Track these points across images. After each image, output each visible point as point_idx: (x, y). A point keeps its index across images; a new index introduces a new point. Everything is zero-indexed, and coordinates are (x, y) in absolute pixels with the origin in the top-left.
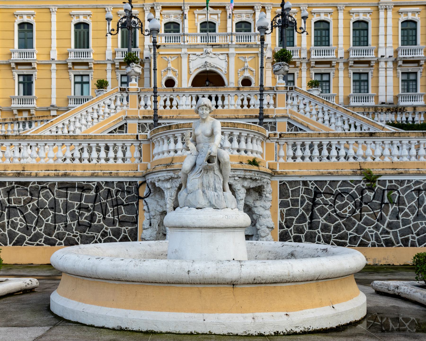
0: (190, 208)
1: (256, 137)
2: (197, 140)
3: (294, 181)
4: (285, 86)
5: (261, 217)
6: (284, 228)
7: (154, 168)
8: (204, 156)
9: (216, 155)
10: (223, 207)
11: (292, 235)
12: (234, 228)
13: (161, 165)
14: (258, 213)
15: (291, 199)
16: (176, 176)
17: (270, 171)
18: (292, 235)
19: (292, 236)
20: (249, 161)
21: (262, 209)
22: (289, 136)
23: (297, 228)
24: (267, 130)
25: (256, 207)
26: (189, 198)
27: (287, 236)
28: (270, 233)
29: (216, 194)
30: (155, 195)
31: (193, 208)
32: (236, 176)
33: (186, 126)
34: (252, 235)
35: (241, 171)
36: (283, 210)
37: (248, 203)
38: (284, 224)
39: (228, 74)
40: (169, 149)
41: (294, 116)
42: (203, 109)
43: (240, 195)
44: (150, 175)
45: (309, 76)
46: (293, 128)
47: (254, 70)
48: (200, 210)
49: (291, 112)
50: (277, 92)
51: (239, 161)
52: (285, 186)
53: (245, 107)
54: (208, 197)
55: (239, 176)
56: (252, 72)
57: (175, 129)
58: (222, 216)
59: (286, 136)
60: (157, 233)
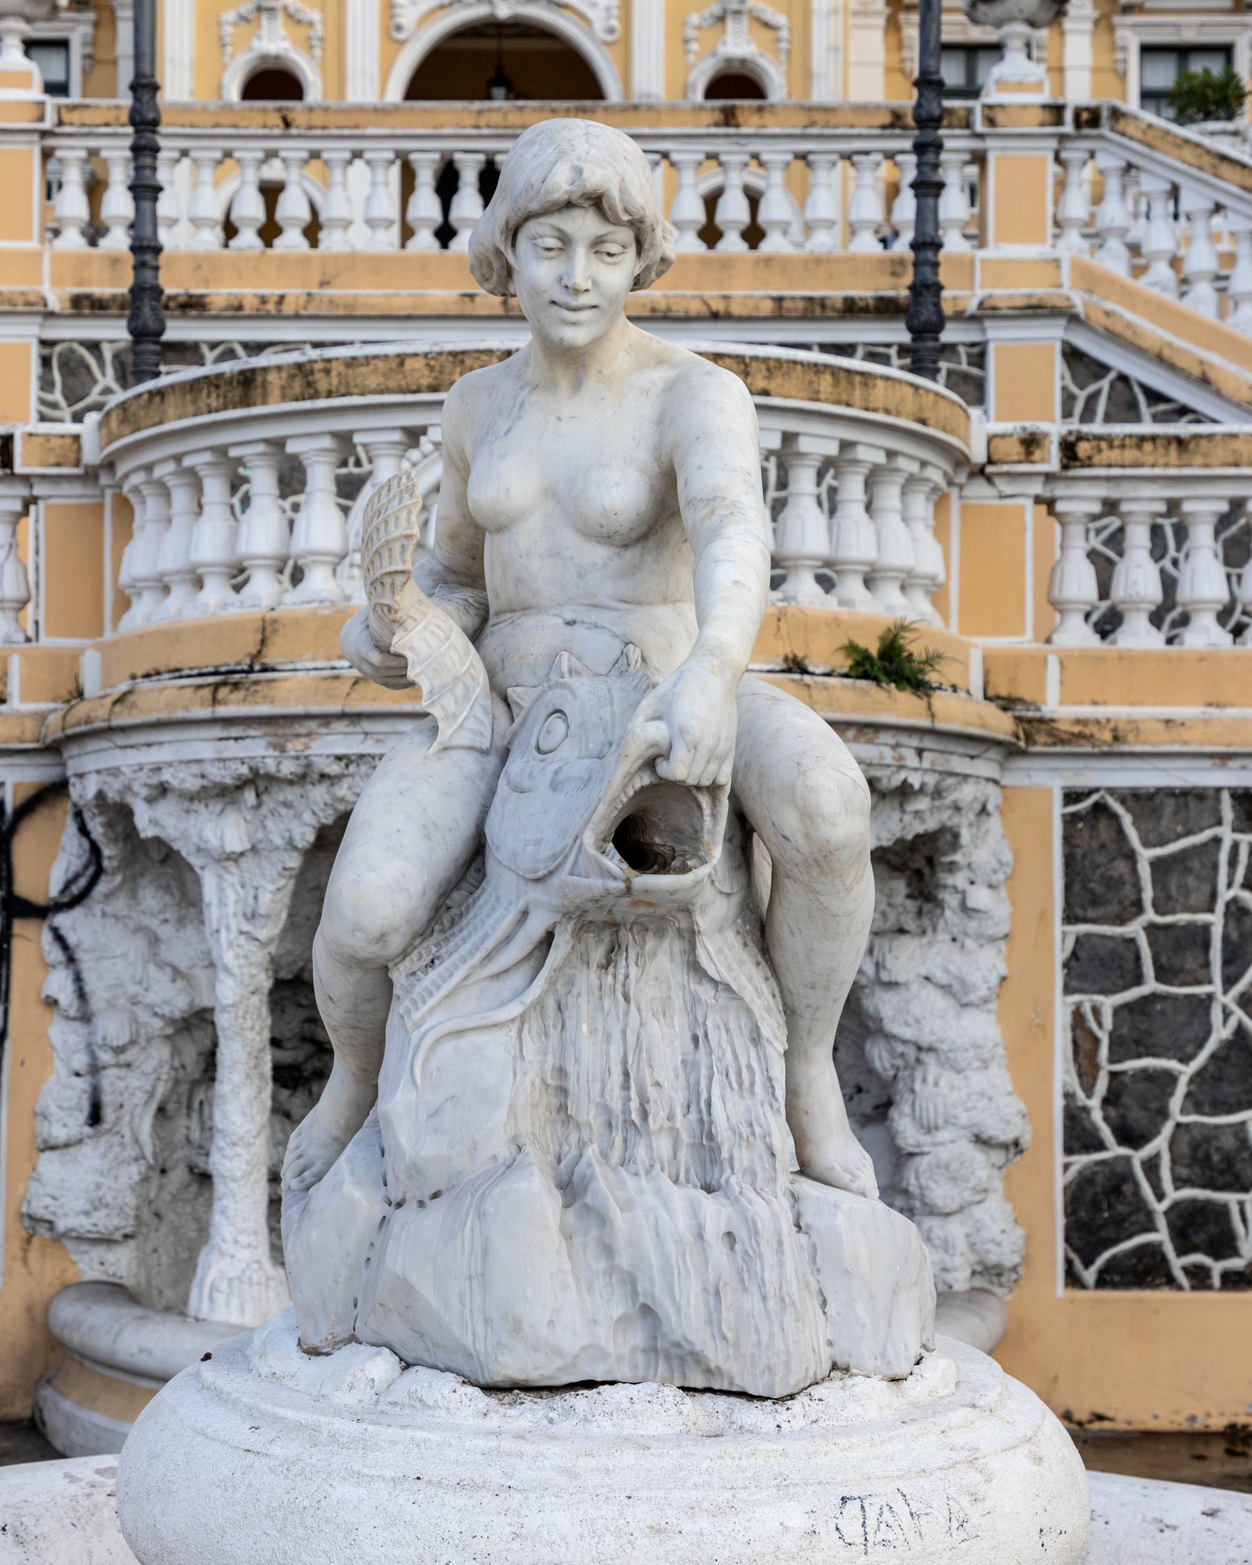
0: (420, 1375)
1: (902, 463)
2: (492, 576)
3: (1170, 792)
4: (1045, 97)
5: (928, 1058)
6: (1101, 1146)
7: (120, 700)
8: (578, 768)
9: (725, 778)
11: (1160, 1196)
13: (176, 672)
14: (907, 1033)
15: (1151, 929)
16: (288, 768)
17: (1001, 724)
18: (1160, 1196)
19: (1160, 1208)
20: (851, 648)
21: (936, 1000)
22: (1130, 455)
23: (1195, 1147)
24: (975, 412)
25: (892, 985)
26: (398, 1259)
27: (1121, 1208)
28: (997, 1184)
29: (715, 1212)
30: (131, 888)
33: (373, 382)
36: (1096, 1011)
38: (1097, 1116)
39: (623, 43)
40: (243, 549)
41: (1109, 306)
42: (566, 241)
44: (92, 745)
45: (1106, 60)
46: (1105, 384)
47: (781, 20)
48: (530, 1412)
49: (1089, 279)
50: (990, 143)
52: (1105, 831)
53: (732, 244)
54: (624, 1261)
56: (767, 35)
57: (284, 398)
58: (797, 1519)
59: (1115, 455)
60: (146, 1179)
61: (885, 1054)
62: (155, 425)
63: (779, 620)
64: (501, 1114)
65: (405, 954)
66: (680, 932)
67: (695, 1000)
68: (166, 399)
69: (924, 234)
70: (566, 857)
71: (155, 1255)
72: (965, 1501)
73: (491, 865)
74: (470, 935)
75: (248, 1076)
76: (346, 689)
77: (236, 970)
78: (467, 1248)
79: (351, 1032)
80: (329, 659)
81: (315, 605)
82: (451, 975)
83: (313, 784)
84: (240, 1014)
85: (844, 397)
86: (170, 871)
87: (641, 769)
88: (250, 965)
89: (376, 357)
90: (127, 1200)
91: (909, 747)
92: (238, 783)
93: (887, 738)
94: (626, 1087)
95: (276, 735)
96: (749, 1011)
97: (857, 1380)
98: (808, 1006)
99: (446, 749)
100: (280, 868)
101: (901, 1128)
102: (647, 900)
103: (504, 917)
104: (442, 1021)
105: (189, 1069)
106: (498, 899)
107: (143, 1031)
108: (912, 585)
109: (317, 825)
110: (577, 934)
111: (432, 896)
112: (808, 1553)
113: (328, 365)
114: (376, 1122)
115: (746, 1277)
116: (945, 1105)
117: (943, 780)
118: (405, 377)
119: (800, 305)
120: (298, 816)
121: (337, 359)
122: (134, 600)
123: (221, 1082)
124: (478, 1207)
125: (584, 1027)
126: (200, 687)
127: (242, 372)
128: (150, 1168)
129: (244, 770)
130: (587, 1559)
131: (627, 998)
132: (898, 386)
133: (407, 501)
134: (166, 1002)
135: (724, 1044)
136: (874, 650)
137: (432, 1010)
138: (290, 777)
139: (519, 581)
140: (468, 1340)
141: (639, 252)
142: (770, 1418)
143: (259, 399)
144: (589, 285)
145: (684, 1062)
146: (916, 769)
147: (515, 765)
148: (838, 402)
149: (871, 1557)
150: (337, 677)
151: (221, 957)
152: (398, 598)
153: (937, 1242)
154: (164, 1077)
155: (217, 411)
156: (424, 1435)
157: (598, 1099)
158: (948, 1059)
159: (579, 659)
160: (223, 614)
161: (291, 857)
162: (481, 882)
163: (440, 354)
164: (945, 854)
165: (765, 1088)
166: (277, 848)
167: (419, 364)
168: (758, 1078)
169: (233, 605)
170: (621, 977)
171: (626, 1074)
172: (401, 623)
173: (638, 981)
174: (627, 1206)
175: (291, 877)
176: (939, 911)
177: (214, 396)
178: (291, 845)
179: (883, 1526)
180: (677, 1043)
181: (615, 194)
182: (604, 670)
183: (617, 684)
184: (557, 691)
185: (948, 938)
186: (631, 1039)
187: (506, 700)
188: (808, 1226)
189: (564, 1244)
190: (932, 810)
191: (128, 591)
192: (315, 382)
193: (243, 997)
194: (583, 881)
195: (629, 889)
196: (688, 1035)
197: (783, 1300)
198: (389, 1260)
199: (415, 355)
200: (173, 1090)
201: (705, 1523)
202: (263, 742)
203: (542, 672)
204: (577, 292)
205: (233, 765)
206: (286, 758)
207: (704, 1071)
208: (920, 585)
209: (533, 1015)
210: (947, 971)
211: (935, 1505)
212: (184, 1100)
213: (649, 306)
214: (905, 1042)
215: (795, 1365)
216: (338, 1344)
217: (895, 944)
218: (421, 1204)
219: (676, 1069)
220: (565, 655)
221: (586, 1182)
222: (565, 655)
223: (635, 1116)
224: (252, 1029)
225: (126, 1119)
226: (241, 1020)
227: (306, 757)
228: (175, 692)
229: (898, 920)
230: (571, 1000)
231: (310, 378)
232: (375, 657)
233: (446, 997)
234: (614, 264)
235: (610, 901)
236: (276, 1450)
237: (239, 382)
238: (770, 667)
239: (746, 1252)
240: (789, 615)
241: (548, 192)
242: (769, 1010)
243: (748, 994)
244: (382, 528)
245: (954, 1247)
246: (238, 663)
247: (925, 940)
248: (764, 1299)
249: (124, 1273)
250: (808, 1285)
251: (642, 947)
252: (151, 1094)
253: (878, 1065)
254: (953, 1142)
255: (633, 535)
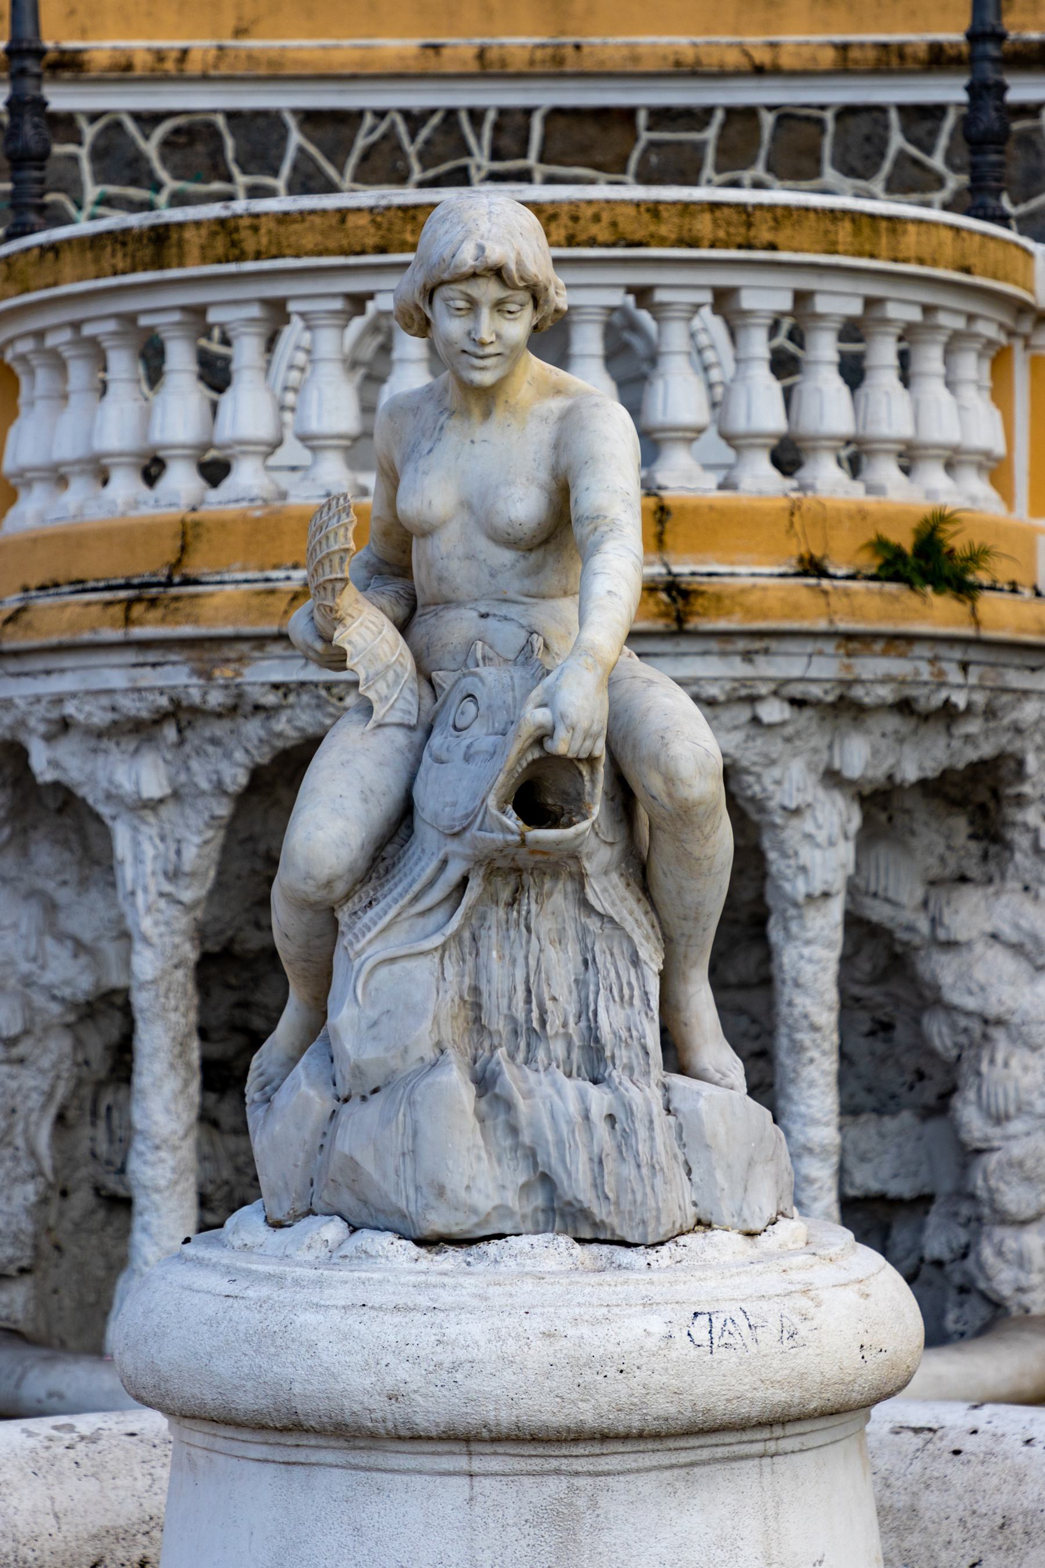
0: (366, 1238)
1: (944, 319)
2: (419, 574)
9: (600, 749)
10: (663, 1231)
12: (770, 1424)
13: (80, 586)
14: (971, 1003)
16: (216, 699)
20: (880, 545)
25: (951, 945)
26: (347, 1142)
29: (599, 1099)
31: (384, 1243)
32: (763, 689)
33: (309, 241)
34: (924, 1201)
35: (810, 646)
37: (878, 912)
40: (158, 436)
42: (473, 305)
43: (807, 855)
48: (451, 1259)
51: (796, 548)
54: (526, 1138)
55: (796, 690)
57: (204, 260)
58: (657, 1325)
60: (44, 1201)
61: (945, 1030)
62: (48, 286)
63: (792, 514)
64: (427, 1024)
65: (347, 897)
66: (571, 875)
67: (585, 930)
68: (62, 255)
69: (982, 23)
70: (476, 816)
71: (56, 1297)
72: (796, 1319)
73: (418, 824)
74: (400, 881)
75: (172, 1066)
76: (283, 605)
77: (155, 940)
78: (401, 1131)
79: (305, 965)
80: (262, 569)
81: (244, 504)
82: (386, 913)
83: (246, 717)
84: (162, 991)
85: (867, 247)
86: (69, 821)
87: (531, 745)
88: (173, 933)
89: (313, 212)
90: (23, 1225)
91: (950, 660)
92: (156, 717)
93: (922, 650)
94: (528, 1001)
95: (200, 660)
96: (630, 939)
97: (715, 1232)
98: (683, 935)
99: (380, 726)
100: (206, 816)
101: (965, 1120)
102: (540, 849)
103: (428, 865)
104: (379, 951)
105: (95, 1066)
106: (423, 851)
107: (38, 1019)
108: (961, 463)
109: (251, 765)
110: (488, 878)
111: (370, 850)
112: (665, 1352)
113: (255, 221)
114: (327, 1037)
115: (624, 1149)
116: (1017, 1090)
117: (996, 698)
118: (347, 236)
119: (871, 54)
120: (228, 755)
121: (266, 214)
122: (22, 494)
123: (140, 1074)
124: (409, 1098)
125: (494, 954)
126: (109, 604)
127: (154, 228)
128: (50, 1186)
129: (164, 701)
130: (494, 1357)
131: (529, 929)
132: (933, 230)
133: (345, 520)
134: (67, 982)
135: (609, 966)
136: (908, 546)
137: (370, 942)
138: (218, 709)
139: (441, 579)
140: (402, 1204)
141: (536, 306)
142: (642, 1259)
143: (175, 260)
144: (493, 338)
145: (576, 981)
146: (960, 687)
147: (437, 740)
148: (860, 254)
149: (716, 1356)
150: (272, 592)
151: (138, 925)
152: (338, 600)
153: (1010, 1256)
154: (65, 1075)
155: (124, 273)
156: (368, 1275)
157: (506, 1011)
158: (1020, 1034)
159: (491, 647)
160: (133, 514)
161: (219, 804)
162: (410, 837)
163: (388, 208)
164: (1010, 784)
165: (642, 1000)
166: (203, 793)
167: (363, 220)
168: (637, 992)
169: (145, 503)
170: (524, 913)
171: (529, 991)
172: (340, 620)
173: (538, 915)
174: (528, 1094)
175: (220, 827)
176: (1007, 854)
177: (120, 255)
178: (219, 789)
179: (726, 1333)
180: (570, 966)
181: (513, 267)
182: (512, 657)
183: (518, 673)
184: (469, 679)
185: (1018, 886)
186: (532, 962)
187: (430, 681)
188: (676, 1110)
189: (478, 1125)
190: (987, 733)
191: (13, 481)
192: (240, 241)
193: (164, 972)
194: (488, 835)
195: (523, 842)
196: (580, 959)
197: (653, 1167)
198: (338, 1143)
199: (359, 210)
200: (74, 1093)
201: (585, 1330)
202: (185, 670)
203: (460, 658)
204: (483, 344)
205: (150, 697)
206: (213, 687)
207: (592, 988)
208: (971, 463)
209: (452, 944)
210: (1017, 927)
211: (770, 1320)
212: (88, 1105)
213: (672, 58)
214: (969, 1014)
215: (663, 1220)
216: (298, 1217)
217: (955, 895)
218: (364, 1098)
219: (570, 986)
220: (480, 644)
221: (496, 1076)
222: (480, 644)
223: (535, 1025)
224: (176, 1009)
225: (20, 1127)
226: (162, 1000)
227: (238, 686)
228: (78, 610)
229: (960, 867)
230: (483, 932)
231: (235, 236)
232: (319, 646)
233: (383, 930)
234: (514, 319)
235: (511, 851)
236: (250, 1293)
237: (150, 239)
238: (777, 570)
239: (624, 1130)
240: (804, 508)
241: (456, 267)
242: (647, 938)
243: (629, 925)
244: (324, 542)
245: (1030, 1262)
246: (154, 574)
247: (991, 890)
248: (639, 1166)
249: (20, 1316)
250: (675, 1157)
251: (541, 888)
252: (50, 1096)
253: (937, 1043)
254: (1028, 1134)
255: (536, 541)
